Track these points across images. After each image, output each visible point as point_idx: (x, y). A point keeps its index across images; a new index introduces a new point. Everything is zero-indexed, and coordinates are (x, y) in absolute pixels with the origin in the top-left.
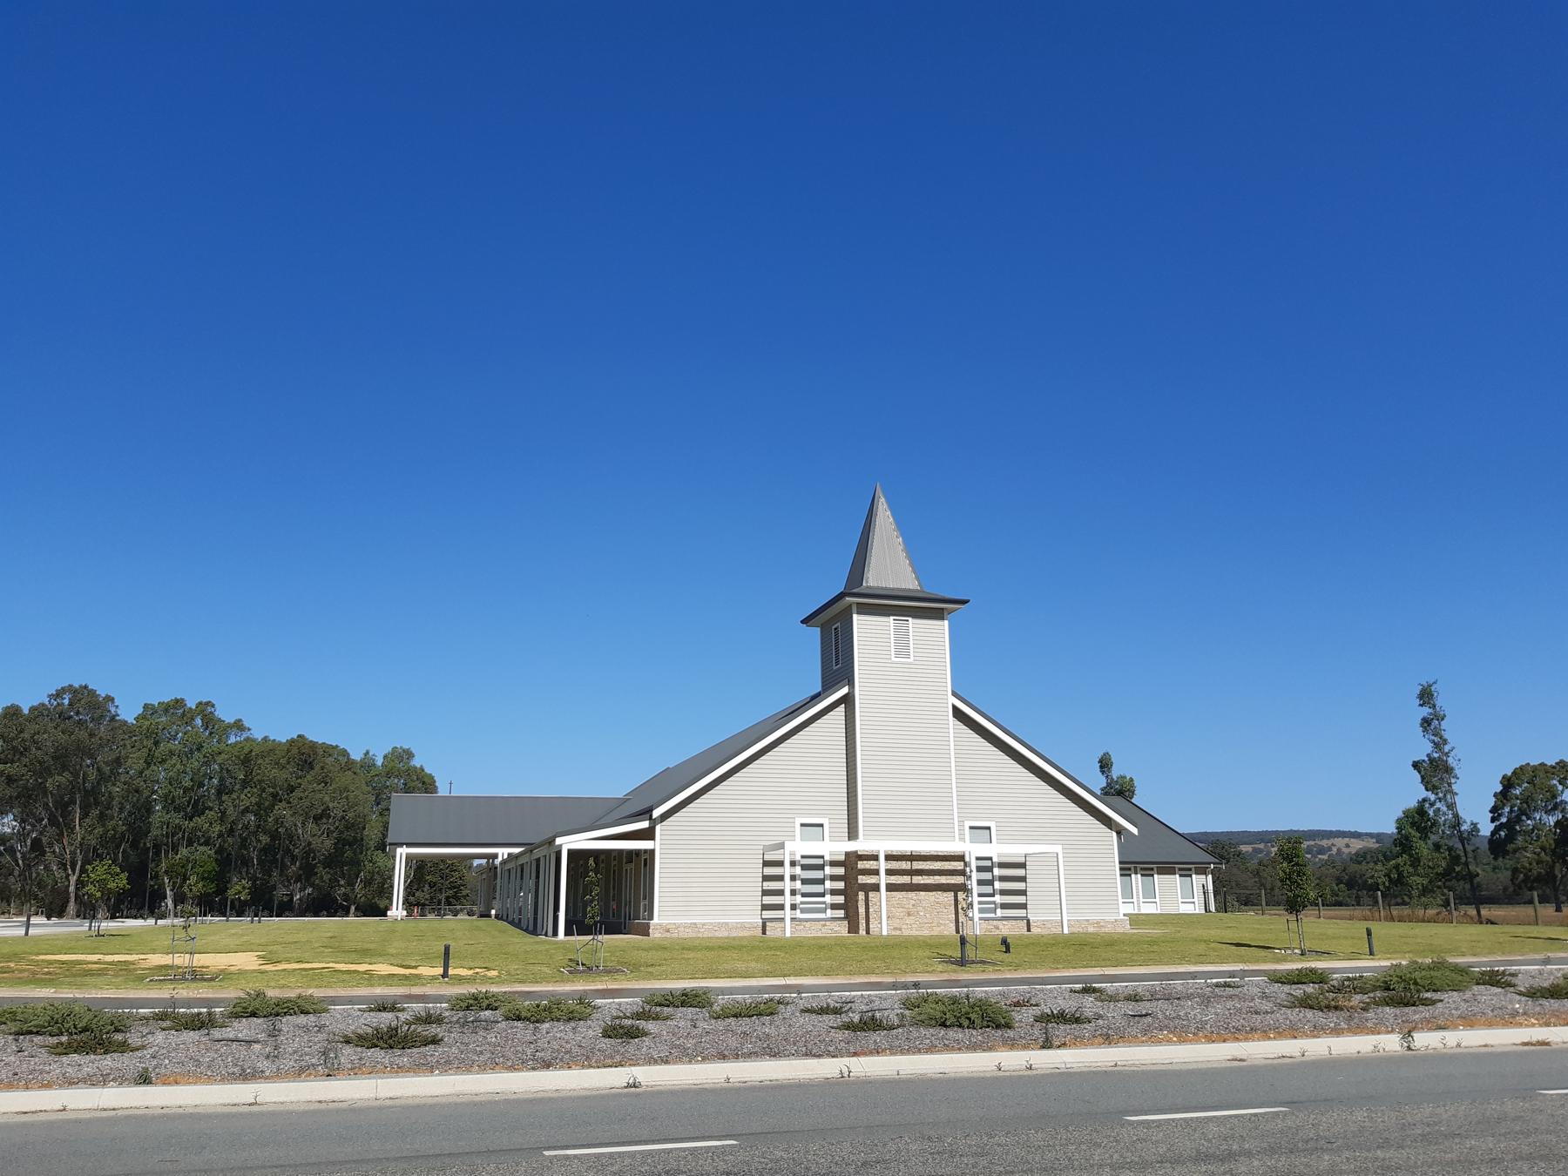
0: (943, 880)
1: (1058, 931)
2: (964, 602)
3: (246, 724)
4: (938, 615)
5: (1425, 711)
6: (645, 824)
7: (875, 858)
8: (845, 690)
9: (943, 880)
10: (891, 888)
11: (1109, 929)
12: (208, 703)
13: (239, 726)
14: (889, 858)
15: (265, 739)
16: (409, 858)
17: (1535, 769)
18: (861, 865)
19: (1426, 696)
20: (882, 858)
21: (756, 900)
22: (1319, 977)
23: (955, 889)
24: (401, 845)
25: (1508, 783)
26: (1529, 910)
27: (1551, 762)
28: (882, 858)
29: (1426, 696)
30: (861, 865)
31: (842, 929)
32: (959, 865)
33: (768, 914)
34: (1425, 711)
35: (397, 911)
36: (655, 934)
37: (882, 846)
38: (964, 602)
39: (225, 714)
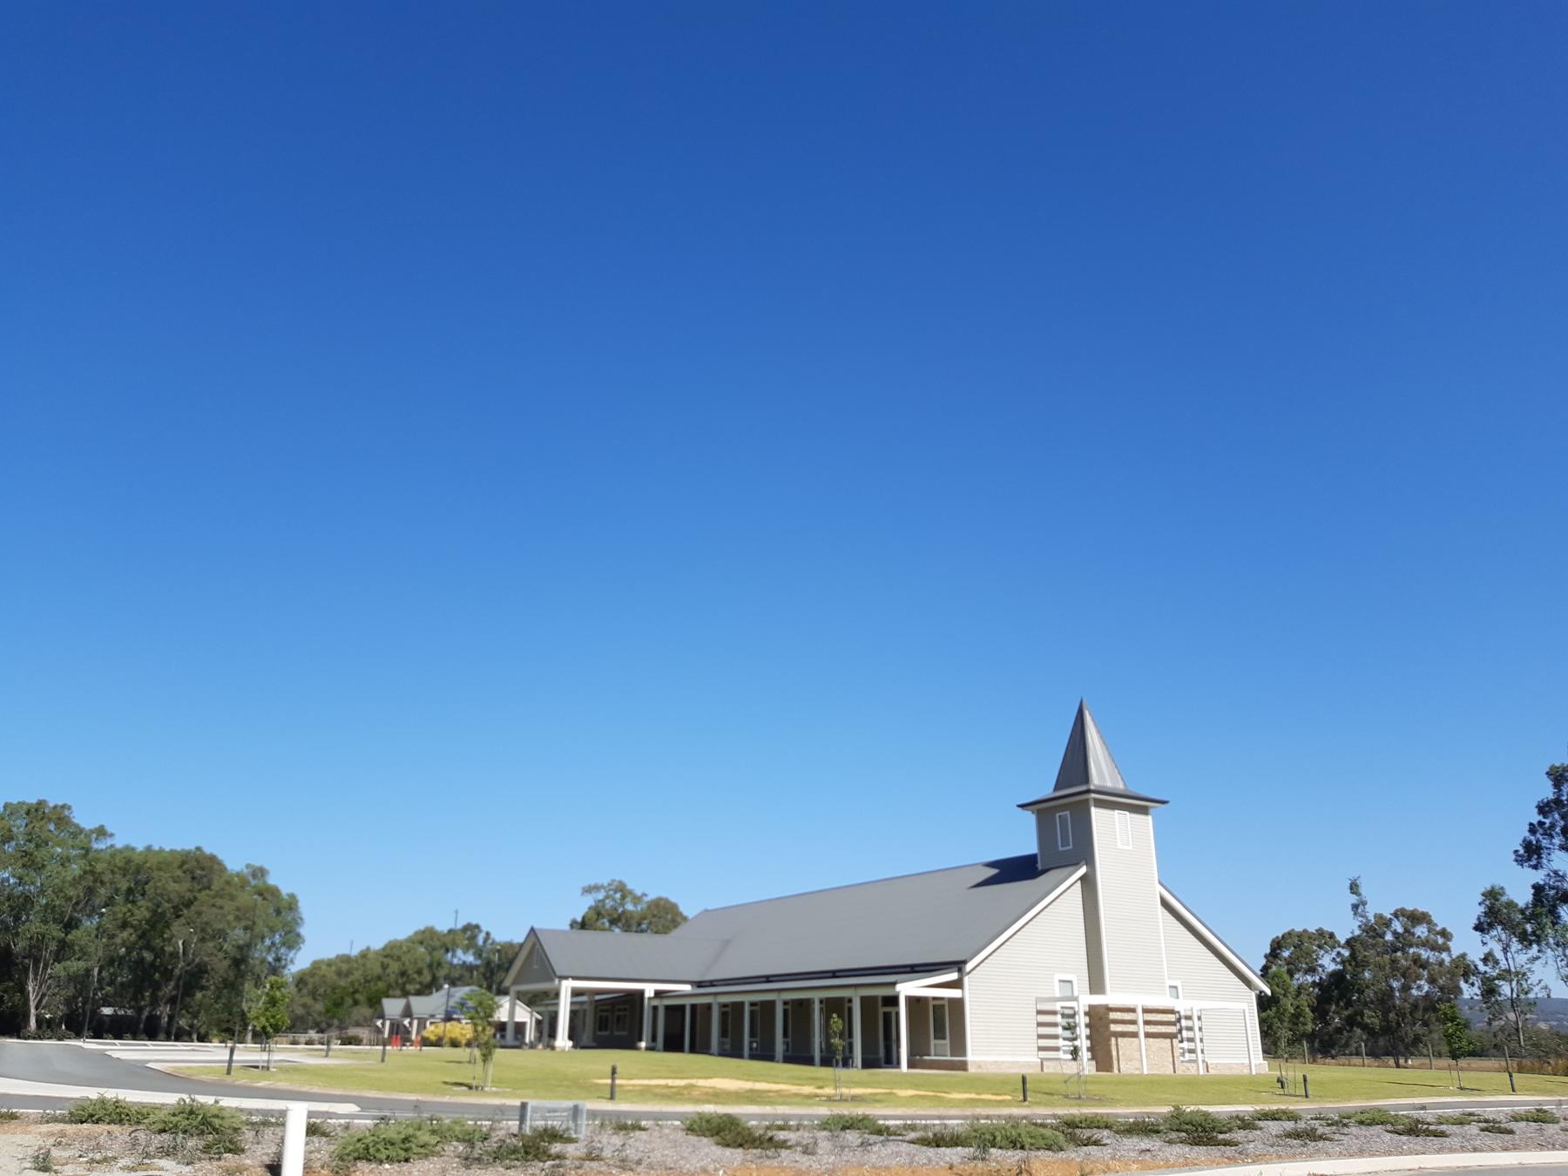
0: (1163, 1029)
1: (1246, 1071)
2: (1163, 802)
3: (109, 829)
4: (1143, 811)
5: (1354, 899)
6: (954, 976)
7: (1133, 1010)
8: (1083, 870)
9: (1163, 1029)
10: (1148, 1035)
11: (1236, 1072)
12: (63, 807)
13: (101, 832)
14: (1145, 1011)
15: (149, 848)
16: (576, 993)
17: (1300, 935)
18: (1113, 1016)
19: (1354, 888)
20: (1140, 1011)
21: (1034, 1043)
22: (1292, 1117)
23: (1171, 1036)
24: (566, 978)
25: (1277, 946)
26: (1426, 1061)
27: (1312, 929)
28: (1140, 1011)
29: (1354, 888)
30: (1113, 1016)
31: (1087, 1066)
32: (1172, 1018)
33: (1044, 1054)
34: (1354, 899)
35: (563, 1041)
36: (972, 1069)
37: (1139, 1000)
38: (1163, 802)
39: (84, 819)
